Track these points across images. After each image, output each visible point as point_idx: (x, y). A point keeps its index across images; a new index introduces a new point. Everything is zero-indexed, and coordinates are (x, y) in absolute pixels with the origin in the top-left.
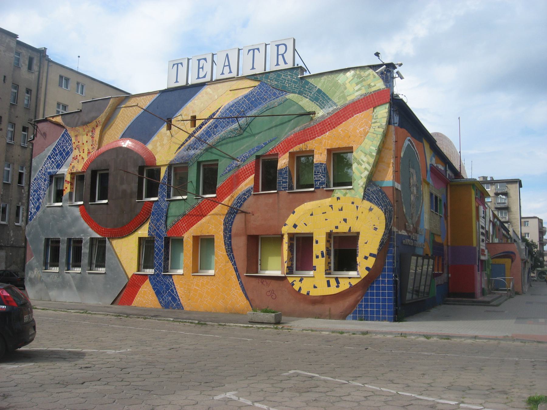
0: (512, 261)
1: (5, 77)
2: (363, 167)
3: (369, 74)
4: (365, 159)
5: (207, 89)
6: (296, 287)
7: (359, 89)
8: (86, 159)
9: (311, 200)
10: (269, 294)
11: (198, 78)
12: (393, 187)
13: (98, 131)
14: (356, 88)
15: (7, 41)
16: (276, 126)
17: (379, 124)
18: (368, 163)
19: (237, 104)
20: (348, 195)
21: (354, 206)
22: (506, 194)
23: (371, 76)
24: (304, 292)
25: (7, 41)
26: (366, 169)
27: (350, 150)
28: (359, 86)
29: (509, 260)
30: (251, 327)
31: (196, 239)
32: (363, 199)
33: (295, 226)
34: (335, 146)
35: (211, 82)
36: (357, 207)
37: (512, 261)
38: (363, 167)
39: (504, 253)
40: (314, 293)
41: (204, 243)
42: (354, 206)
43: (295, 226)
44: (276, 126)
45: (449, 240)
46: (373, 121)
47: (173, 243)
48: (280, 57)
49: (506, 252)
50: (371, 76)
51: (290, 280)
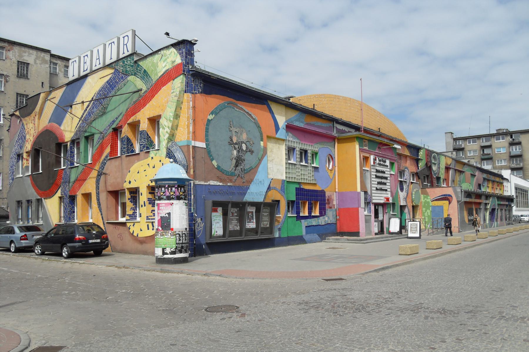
0: (450, 203)
1: (43, 83)
2: (166, 130)
3: (172, 52)
4: (166, 124)
5: (89, 79)
6: (131, 231)
7: (166, 66)
8: (32, 140)
9: (139, 160)
10: (119, 236)
11: (84, 71)
12: (188, 146)
13: (37, 117)
14: (163, 65)
15: (42, 56)
16: (123, 102)
17: (175, 94)
18: (168, 127)
19: (103, 88)
20: (157, 155)
21: (161, 163)
22: (519, 143)
23: (173, 53)
24: (135, 234)
25: (42, 56)
26: (167, 132)
27: (159, 117)
28: (165, 63)
29: (447, 202)
30: (83, 263)
31: (83, 195)
32: (166, 157)
33: (130, 182)
34: (152, 116)
35: (93, 72)
36: (160, 161)
37: (450, 203)
38: (166, 130)
39: (442, 196)
40: (142, 235)
41: (87, 196)
42: (161, 163)
43: (130, 182)
44: (123, 102)
45: (337, 187)
46: (172, 91)
47: (73, 199)
48: (125, 46)
49: (444, 195)
50: (173, 53)
51: (128, 225)
